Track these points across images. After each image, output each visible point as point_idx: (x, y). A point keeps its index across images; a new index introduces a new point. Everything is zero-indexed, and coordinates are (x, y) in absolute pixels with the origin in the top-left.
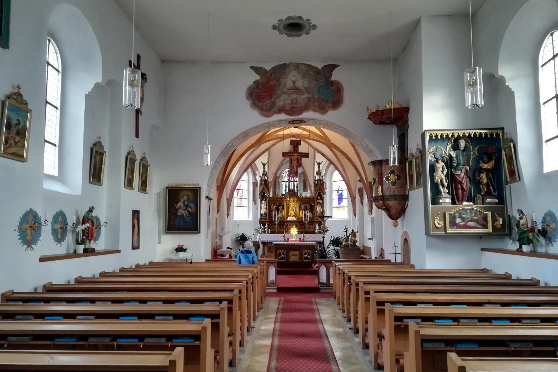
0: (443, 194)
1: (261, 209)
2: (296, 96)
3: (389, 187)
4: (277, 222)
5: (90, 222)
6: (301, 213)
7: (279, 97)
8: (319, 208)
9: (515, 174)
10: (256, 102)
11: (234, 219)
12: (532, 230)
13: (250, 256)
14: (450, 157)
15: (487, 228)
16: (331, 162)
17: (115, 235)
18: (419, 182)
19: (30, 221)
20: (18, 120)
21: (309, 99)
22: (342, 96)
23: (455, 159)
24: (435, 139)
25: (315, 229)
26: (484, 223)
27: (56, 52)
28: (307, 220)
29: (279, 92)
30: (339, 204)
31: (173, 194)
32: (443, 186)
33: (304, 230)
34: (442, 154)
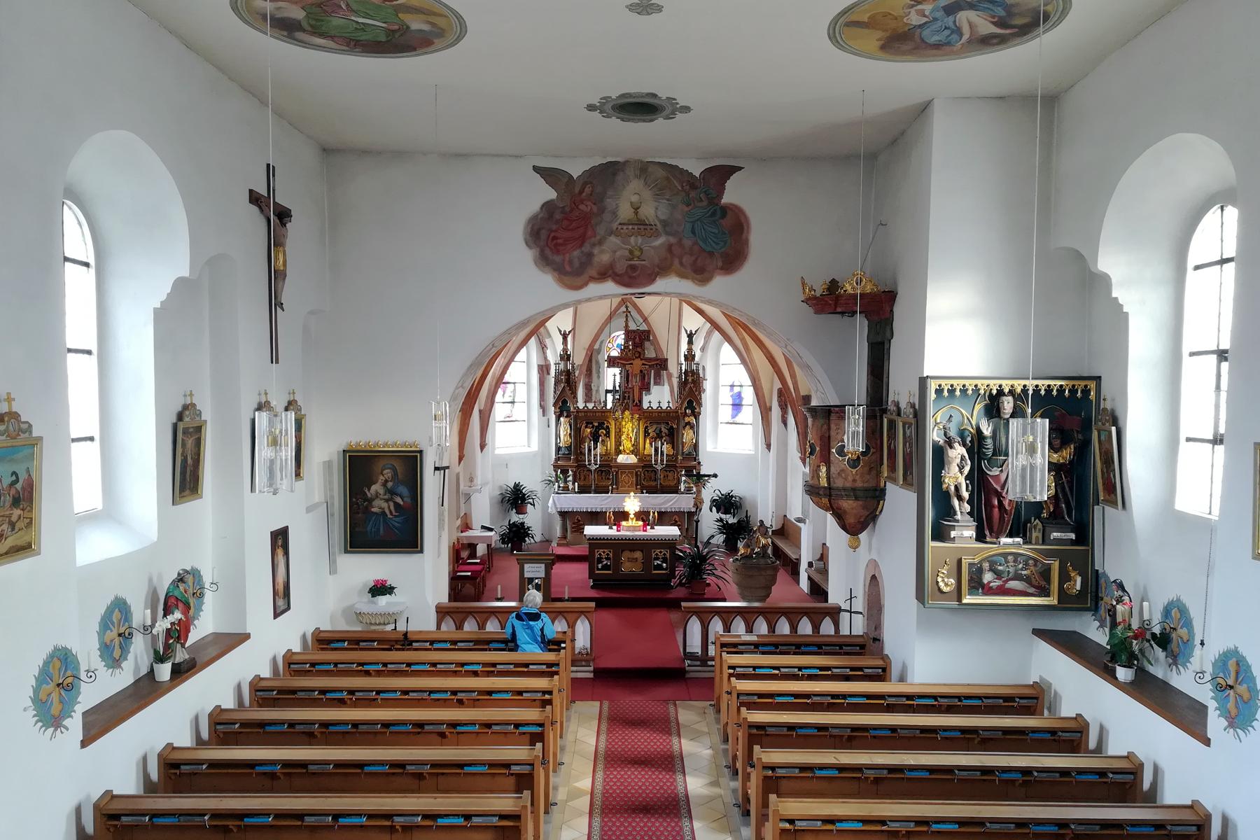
0: (959, 517)
1: (558, 436)
2: (640, 240)
3: (843, 470)
4: (593, 467)
5: (181, 605)
6: (647, 445)
7: (600, 243)
8: (688, 436)
9: (1114, 491)
10: (548, 251)
11: (497, 452)
12: (1140, 635)
13: (537, 625)
14: (979, 430)
15: (1048, 595)
16: (715, 326)
17: (237, 600)
18: (909, 478)
19: (55, 677)
20: (14, 473)
21: (670, 248)
22: (746, 242)
23: (989, 441)
24: (948, 394)
25: (679, 482)
26: (1043, 583)
27: (79, 224)
28: (662, 460)
29: (601, 231)
30: (734, 417)
31: (360, 466)
32: (960, 498)
33: (653, 484)
34: (963, 424)
